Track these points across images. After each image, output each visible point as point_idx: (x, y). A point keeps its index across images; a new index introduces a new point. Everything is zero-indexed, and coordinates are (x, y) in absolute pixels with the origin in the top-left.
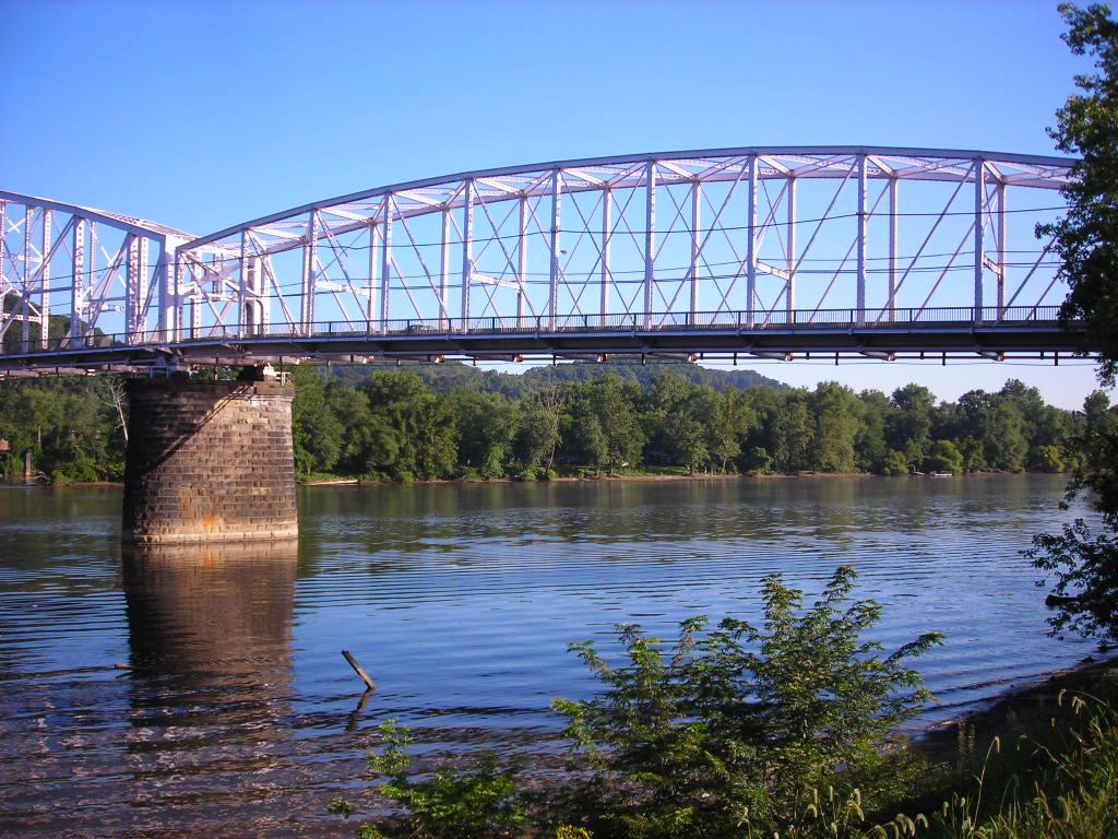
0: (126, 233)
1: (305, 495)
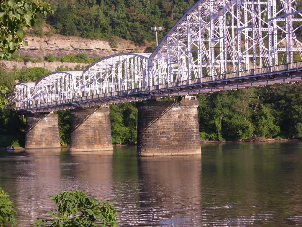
0: (82, 72)
1: (27, 114)
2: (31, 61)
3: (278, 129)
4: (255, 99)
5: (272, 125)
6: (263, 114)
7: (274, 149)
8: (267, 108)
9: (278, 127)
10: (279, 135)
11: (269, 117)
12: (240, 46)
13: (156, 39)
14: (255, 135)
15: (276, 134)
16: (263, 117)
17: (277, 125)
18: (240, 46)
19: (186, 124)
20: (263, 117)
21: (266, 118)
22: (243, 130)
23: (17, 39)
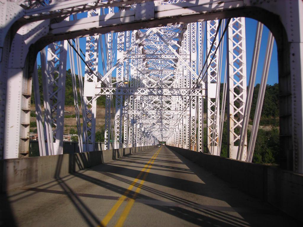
2: (178, 37)
3: (273, 159)
4: (264, 145)
5: (271, 157)
6: (266, 152)
7: (120, 18)
8: (269, 149)
9: (274, 158)
10: (274, 162)
11: (269, 153)
12: (128, 44)
13: (223, 127)
14: (263, 162)
15: (272, 162)
16: (267, 154)
17: (273, 157)
18: (128, 44)
19: (160, 57)
20: (267, 154)
21: (268, 154)
22: (256, 159)
23: (149, 84)
